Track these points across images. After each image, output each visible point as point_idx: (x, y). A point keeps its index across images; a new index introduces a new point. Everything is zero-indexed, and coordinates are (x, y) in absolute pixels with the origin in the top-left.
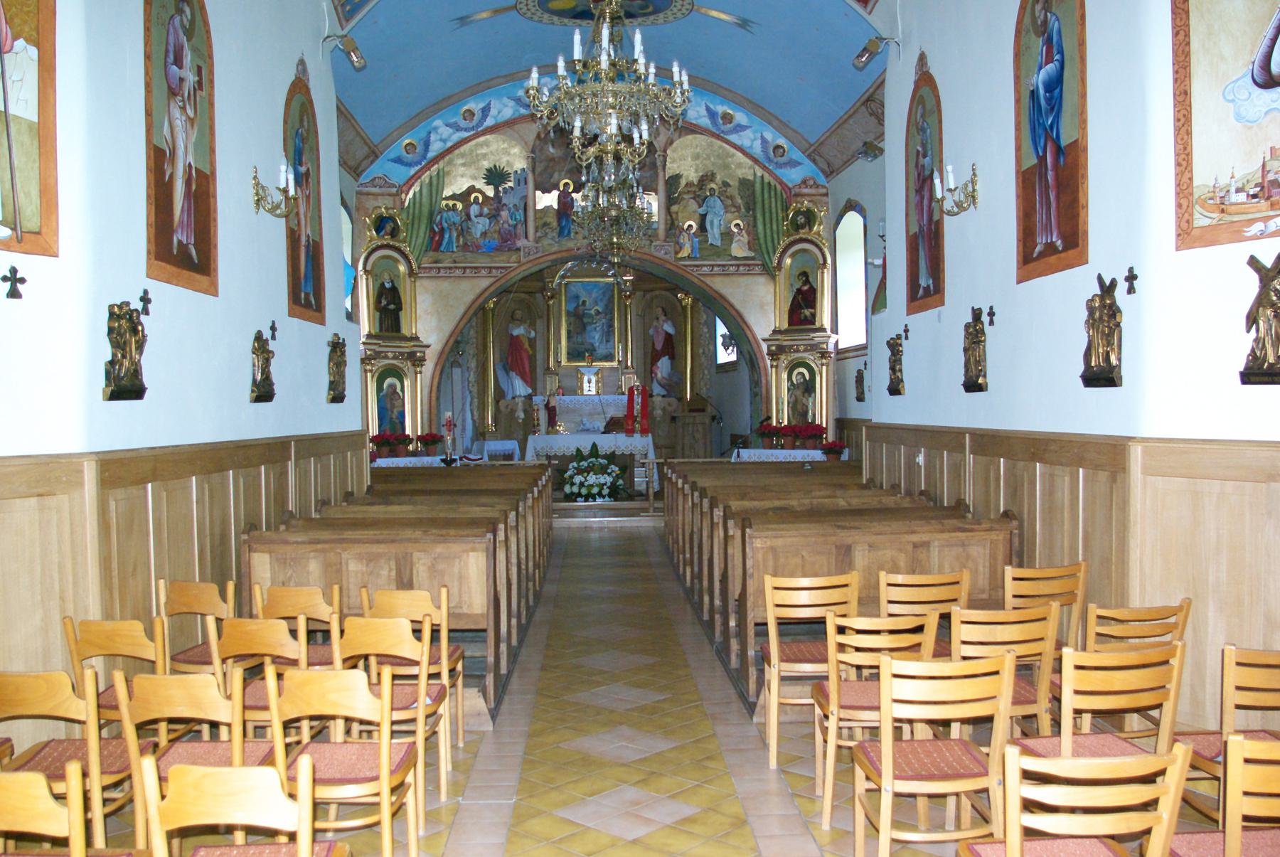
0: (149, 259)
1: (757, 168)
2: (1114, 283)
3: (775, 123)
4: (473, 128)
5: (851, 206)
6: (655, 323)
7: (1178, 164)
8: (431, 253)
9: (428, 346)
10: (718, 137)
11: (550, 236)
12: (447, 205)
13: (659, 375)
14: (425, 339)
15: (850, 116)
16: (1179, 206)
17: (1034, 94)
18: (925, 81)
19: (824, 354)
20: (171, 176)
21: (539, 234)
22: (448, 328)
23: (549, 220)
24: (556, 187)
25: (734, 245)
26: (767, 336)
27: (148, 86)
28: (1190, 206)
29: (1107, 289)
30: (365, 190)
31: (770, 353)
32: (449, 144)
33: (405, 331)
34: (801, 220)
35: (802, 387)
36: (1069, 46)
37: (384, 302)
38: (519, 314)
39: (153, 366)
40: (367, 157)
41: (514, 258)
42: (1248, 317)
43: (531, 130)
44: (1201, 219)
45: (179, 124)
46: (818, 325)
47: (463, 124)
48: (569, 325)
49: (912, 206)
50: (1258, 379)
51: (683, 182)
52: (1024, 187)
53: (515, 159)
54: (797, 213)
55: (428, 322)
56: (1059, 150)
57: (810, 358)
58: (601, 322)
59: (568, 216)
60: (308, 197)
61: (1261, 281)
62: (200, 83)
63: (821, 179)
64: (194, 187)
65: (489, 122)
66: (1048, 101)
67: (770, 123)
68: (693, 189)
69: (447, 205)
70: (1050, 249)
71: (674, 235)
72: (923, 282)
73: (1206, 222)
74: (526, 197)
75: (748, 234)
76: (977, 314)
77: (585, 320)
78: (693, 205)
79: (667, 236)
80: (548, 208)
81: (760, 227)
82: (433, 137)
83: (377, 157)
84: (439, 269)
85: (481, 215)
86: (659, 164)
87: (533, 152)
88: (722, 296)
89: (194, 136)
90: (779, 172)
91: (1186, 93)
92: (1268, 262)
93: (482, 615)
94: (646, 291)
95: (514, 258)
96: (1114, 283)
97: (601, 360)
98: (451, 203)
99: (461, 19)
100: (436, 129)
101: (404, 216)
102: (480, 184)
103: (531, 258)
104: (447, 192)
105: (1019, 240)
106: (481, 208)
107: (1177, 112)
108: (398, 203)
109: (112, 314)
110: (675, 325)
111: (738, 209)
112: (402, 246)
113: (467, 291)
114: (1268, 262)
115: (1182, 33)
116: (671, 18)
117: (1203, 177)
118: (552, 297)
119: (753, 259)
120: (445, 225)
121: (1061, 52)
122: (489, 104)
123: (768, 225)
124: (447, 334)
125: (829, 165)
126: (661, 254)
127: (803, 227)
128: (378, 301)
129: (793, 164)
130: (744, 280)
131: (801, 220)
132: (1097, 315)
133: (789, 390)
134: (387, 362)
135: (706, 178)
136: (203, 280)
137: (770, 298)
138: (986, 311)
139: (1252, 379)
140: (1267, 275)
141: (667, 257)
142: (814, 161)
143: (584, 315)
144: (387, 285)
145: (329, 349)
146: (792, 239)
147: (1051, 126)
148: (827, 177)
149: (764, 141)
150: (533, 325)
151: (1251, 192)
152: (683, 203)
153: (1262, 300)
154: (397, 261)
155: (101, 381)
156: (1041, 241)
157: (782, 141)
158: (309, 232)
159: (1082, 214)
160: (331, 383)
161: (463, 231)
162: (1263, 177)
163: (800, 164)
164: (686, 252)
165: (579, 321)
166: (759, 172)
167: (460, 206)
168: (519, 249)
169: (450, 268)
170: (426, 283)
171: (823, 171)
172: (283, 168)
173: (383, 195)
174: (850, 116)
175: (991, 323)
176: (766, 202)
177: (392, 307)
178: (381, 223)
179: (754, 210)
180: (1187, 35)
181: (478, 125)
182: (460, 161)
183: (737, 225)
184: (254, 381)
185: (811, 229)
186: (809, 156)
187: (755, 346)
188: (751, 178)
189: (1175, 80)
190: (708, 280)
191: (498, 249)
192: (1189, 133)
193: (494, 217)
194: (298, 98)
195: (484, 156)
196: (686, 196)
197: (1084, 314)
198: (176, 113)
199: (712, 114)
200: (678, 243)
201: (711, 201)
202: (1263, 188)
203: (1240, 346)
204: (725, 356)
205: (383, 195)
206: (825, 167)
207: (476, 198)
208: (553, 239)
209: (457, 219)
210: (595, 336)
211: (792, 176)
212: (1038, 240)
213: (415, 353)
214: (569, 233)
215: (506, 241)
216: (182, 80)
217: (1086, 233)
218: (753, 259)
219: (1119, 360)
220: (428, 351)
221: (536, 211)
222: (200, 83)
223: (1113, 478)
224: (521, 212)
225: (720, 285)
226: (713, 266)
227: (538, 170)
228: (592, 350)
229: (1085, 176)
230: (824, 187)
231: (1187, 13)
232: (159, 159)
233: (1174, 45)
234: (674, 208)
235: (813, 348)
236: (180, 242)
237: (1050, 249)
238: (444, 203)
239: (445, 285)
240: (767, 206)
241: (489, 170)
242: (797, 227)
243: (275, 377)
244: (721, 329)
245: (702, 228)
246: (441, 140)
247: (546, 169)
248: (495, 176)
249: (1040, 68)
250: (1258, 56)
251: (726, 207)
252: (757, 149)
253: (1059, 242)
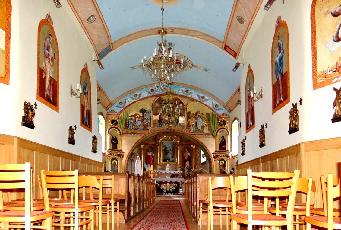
0: (37, 95)
1: (211, 110)
2: (296, 104)
3: (216, 99)
4: (137, 99)
5: (235, 119)
6: (185, 153)
7: (313, 67)
8: (126, 130)
9: (124, 153)
10: (201, 102)
11: (157, 126)
12: (130, 118)
13: (187, 166)
14: (123, 151)
15: (235, 95)
16: (313, 78)
17: (276, 64)
18: (250, 71)
19: (228, 157)
20: (45, 77)
21: (154, 126)
22: (130, 149)
23: (156, 122)
24: (158, 114)
25: (205, 130)
26: (213, 153)
27: (39, 52)
28: (317, 78)
29: (295, 106)
30: (109, 113)
31: (214, 157)
32: (131, 103)
33: (118, 149)
34: (222, 123)
35: (222, 166)
36: (285, 48)
37: (113, 141)
38: (150, 150)
39: (36, 121)
40: (109, 105)
41: (147, 132)
42: (333, 104)
43: (152, 100)
44: (320, 81)
45: (48, 65)
46: (227, 150)
47: (134, 98)
48: (163, 153)
49: (247, 104)
50: (336, 120)
51: (191, 113)
52: (274, 90)
53: (148, 107)
54: (221, 121)
55: (126, 146)
56: (282, 75)
57: (225, 158)
58: (171, 153)
59: (161, 121)
60: (87, 99)
61: (337, 93)
62: (55, 58)
63: (228, 113)
64: (52, 83)
65: (141, 97)
66: (280, 64)
67: (214, 99)
68: (194, 115)
69: (130, 118)
70: (281, 102)
71: (189, 127)
72: (249, 124)
73: (321, 81)
74: (150, 116)
75: (208, 127)
76: (263, 126)
77: (167, 152)
78: (194, 119)
79: (187, 127)
80: (156, 119)
81: (212, 125)
82: (127, 101)
83: (112, 105)
84: (128, 134)
85: (139, 121)
86: (185, 109)
87: (152, 105)
88: (201, 143)
89: (52, 70)
90: (217, 111)
91: (315, 48)
92: (338, 88)
93: (125, 195)
94: (183, 145)
95: (147, 132)
96: (296, 104)
97: (171, 162)
98: (131, 117)
99: (132, 67)
100: (127, 99)
101: (119, 120)
102: (139, 113)
103: (152, 131)
104: (130, 115)
105: (273, 103)
106: (139, 119)
107: (312, 53)
108: (118, 117)
109: (25, 104)
110: (190, 153)
111: (206, 120)
112: (118, 127)
113: (135, 139)
114: (338, 88)
115: (314, 32)
116: (187, 69)
117: (320, 69)
118: (158, 146)
119: (209, 133)
120: (130, 123)
121: (283, 49)
122: (141, 93)
123: (214, 125)
124: (130, 150)
125: (230, 109)
126: (186, 131)
127: (222, 125)
128: (112, 141)
129: (220, 109)
130: (207, 138)
131: (222, 123)
132: (292, 114)
133: (219, 166)
134: (113, 156)
135: (197, 113)
136: (54, 107)
137: (214, 143)
138: (265, 124)
139: (335, 121)
140: (338, 91)
141: (187, 132)
142: (226, 109)
143: (167, 151)
144: (114, 137)
145: (92, 139)
146: (220, 128)
147: (280, 70)
148: (229, 112)
149: (213, 103)
150: (153, 152)
151: (334, 71)
152: (191, 119)
153: (337, 99)
154: (117, 131)
155: (21, 121)
156: (278, 101)
157: (217, 103)
158: (87, 107)
159: (288, 89)
160: (93, 147)
161: (134, 125)
162: (337, 66)
163: (222, 109)
164: (192, 131)
165: (166, 152)
166: (211, 111)
167: (133, 118)
168: (148, 129)
169: (131, 134)
170: (125, 137)
171: (228, 111)
172: (78, 84)
173: (113, 115)
174: (235, 95)
175: (266, 127)
176: (213, 119)
177: (115, 142)
178: (113, 122)
179: (210, 121)
180: (315, 32)
181: (139, 98)
182: (133, 107)
183: (205, 124)
184: (69, 138)
185: (225, 125)
186: (225, 107)
187: (210, 155)
188: (209, 113)
189: (312, 45)
190: (198, 139)
191: (143, 129)
192: (316, 58)
193: (142, 121)
194: (84, 74)
195: (140, 106)
196: (192, 117)
197: (289, 115)
198: (47, 62)
199: (199, 97)
200: (190, 129)
201: (199, 118)
202: (337, 69)
203: (331, 112)
204: (203, 160)
205: (113, 115)
206: (229, 110)
207: (138, 116)
208: (157, 127)
209: (133, 122)
210: (170, 156)
211: (220, 112)
212: (278, 101)
213: (121, 154)
214: (162, 126)
215: (145, 127)
216: (49, 55)
217: (289, 94)
218: (209, 133)
219: (298, 124)
220: (124, 154)
221: (153, 120)
222: (55, 58)
223: (297, 156)
224: (149, 120)
225: (201, 140)
226: (199, 135)
227: (154, 110)
228: (169, 159)
229: (289, 79)
230: (228, 115)
231: (315, 27)
232: (41, 73)
233: (311, 36)
234: (189, 120)
235: (225, 155)
236: (47, 95)
237: (281, 102)
238: (129, 117)
239: (129, 138)
240: (213, 120)
241: (141, 110)
242: (221, 125)
243: (75, 138)
244: (202, 153)
245: (196, 125)
246: (129, 102)
247: (155, 110)
248: (143, 111)
249: (278, 56)
250: (335, 34)
251: (203, 120)
252: (211, 106)
253: (283, 99)
